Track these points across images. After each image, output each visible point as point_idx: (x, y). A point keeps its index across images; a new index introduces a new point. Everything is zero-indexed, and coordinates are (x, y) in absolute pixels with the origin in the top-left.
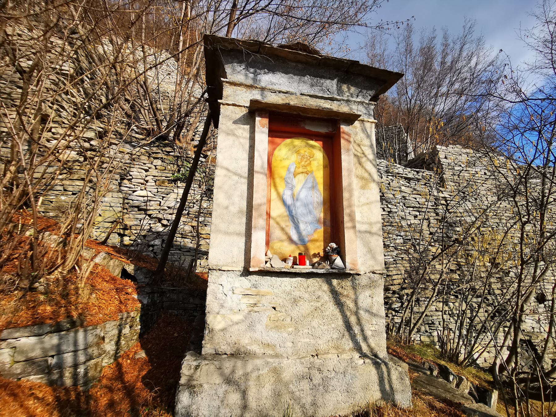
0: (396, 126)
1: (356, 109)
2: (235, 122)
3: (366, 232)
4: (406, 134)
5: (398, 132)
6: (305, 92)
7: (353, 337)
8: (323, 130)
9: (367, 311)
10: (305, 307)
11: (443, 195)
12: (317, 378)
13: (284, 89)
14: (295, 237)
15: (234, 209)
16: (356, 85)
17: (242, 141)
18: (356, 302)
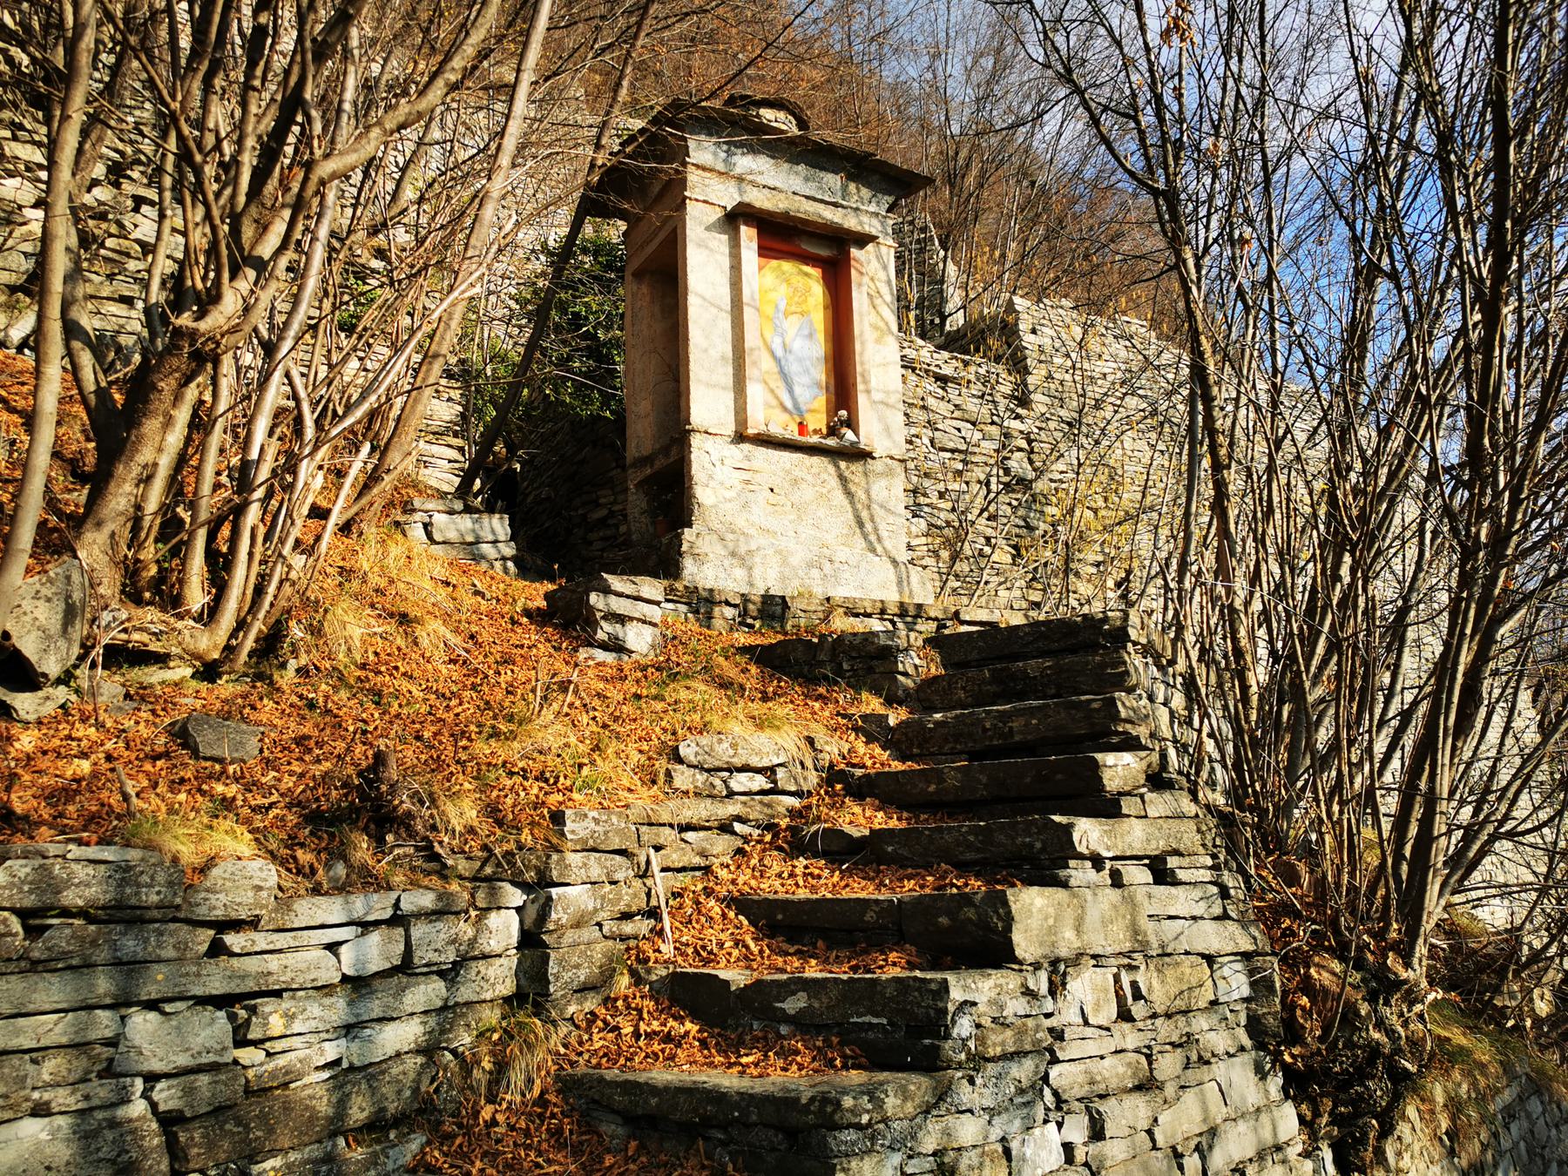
0: (911, 223)
1: (870, 226)
2: (708, 229)
3: (882, 402)
4: (942, 253)
5: (918, 242)
6: (797, 189)
7: (865, 536)
8: (824, 252)
9: (882, 506)
10: (807, 493)
11: (1022, 427)
12: (827, 566)
13: (771, 183)
14: (789, 404)
15: (715, 353)
16: (869, 186)
17: (718, 257)
18: (868, 492)
